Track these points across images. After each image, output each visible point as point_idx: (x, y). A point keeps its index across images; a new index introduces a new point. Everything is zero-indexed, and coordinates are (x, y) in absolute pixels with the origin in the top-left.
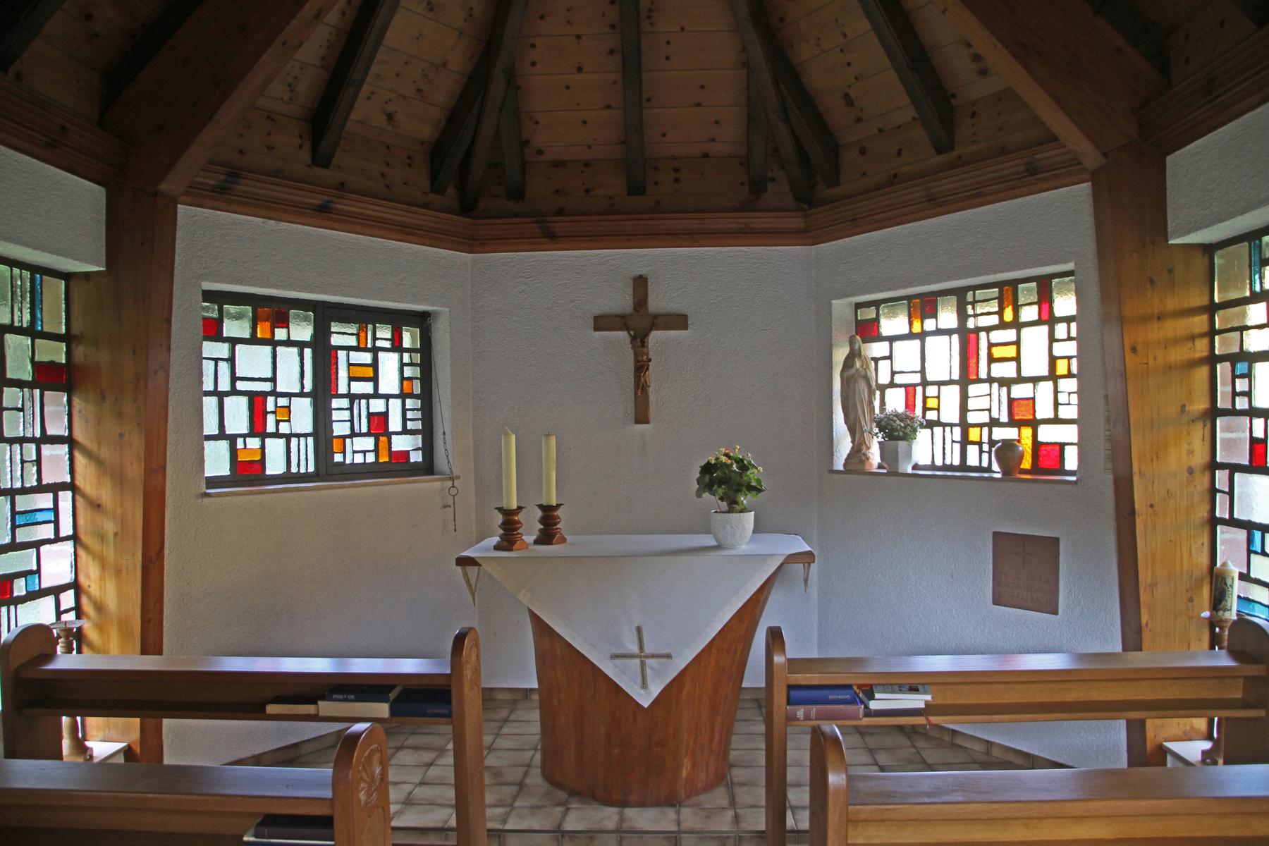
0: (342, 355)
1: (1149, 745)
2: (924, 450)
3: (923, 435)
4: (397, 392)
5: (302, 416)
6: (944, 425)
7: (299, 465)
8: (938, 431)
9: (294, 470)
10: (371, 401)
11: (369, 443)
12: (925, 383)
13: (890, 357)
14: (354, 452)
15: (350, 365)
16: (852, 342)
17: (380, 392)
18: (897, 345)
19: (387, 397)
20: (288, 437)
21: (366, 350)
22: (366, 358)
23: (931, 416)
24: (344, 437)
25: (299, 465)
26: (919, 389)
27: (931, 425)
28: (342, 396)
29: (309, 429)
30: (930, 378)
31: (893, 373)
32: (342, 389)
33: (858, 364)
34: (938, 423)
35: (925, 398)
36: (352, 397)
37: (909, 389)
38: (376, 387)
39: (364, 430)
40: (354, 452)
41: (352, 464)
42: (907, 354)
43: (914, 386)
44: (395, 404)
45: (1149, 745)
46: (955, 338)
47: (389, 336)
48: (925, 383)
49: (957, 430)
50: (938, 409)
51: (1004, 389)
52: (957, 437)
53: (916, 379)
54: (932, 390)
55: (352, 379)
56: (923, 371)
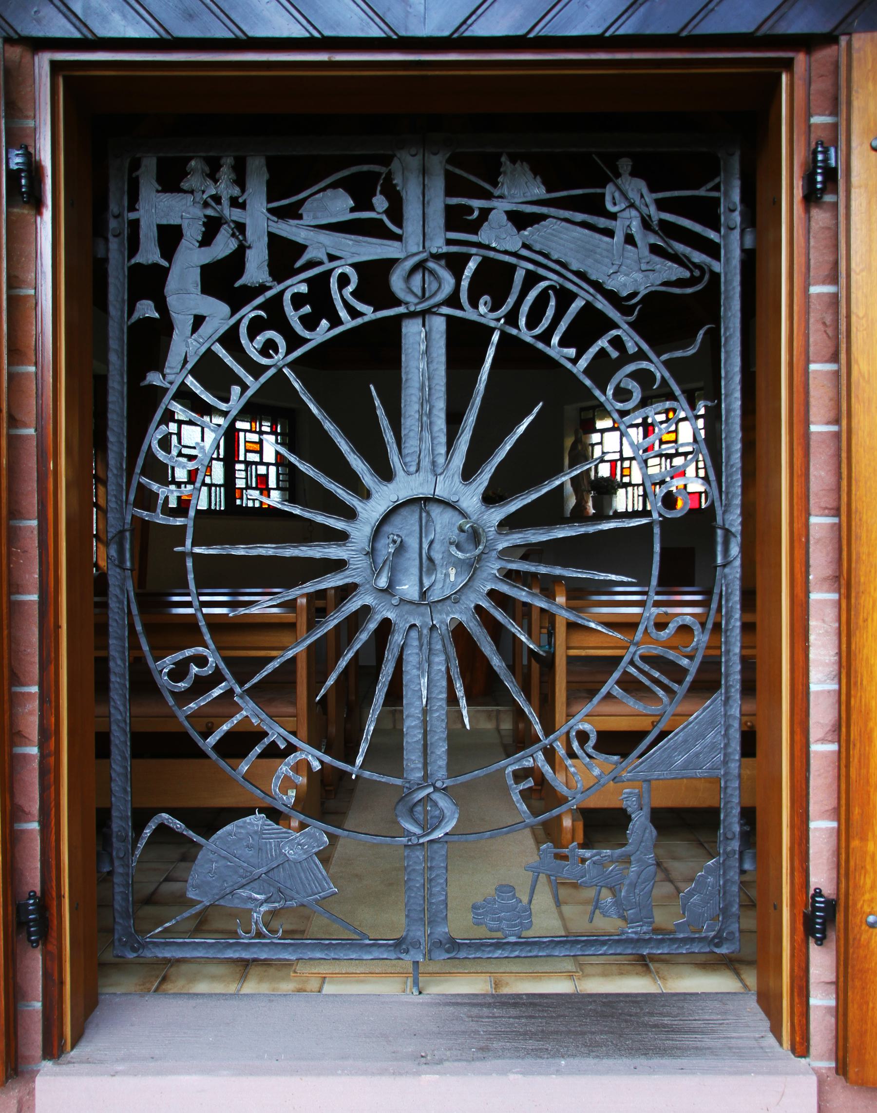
0: (242, 434)
1: (300, 212)
2: (622, 501)
3: (621, 492)
4: (274, 462)
5: (218, 473)
6: (634, 485)
7: (216, 504)
8: (630, 489)
9: (213, 507)
10: (259, 467)
11: (255, 494)
12: (622, 459)
13: (601, 443)
14: (248, 499)
15: (246, 442)
16: (576, 433)
17: (264, 461)
18: (606, 435)
19: (268, 465)
20: (210, 486)
21: (255, 432)
22: (255, 437)
23: (626, 480)
24: (242, 489)
25: (216, 504)
26: (619, 463)
27: (626, 485)
28: (241, 462)
29: (221, 482)
30: (625, 456)
31: (603, 453)
32: (242, 458)
33: (580, 448)
34: (629, 484)
35: (622, 469)
36: (248, 464)
37: (613, 463)
38: (261, 457)
39: (254, 485)
40: (248, 499)
41: (247, 507)
42: (612, 441)
43: (616, 461)
44: (273, 470)
45: (300, 212)
46: (641, 429)
47: (269, 424)
48: (622, 459)
49: (641, 488)
50: (630, 475)
51: (668, 460)
52: (641, 493)
53: (617, 456)
54: (626, 464)
55: (247, 451)
56: (621, 452)
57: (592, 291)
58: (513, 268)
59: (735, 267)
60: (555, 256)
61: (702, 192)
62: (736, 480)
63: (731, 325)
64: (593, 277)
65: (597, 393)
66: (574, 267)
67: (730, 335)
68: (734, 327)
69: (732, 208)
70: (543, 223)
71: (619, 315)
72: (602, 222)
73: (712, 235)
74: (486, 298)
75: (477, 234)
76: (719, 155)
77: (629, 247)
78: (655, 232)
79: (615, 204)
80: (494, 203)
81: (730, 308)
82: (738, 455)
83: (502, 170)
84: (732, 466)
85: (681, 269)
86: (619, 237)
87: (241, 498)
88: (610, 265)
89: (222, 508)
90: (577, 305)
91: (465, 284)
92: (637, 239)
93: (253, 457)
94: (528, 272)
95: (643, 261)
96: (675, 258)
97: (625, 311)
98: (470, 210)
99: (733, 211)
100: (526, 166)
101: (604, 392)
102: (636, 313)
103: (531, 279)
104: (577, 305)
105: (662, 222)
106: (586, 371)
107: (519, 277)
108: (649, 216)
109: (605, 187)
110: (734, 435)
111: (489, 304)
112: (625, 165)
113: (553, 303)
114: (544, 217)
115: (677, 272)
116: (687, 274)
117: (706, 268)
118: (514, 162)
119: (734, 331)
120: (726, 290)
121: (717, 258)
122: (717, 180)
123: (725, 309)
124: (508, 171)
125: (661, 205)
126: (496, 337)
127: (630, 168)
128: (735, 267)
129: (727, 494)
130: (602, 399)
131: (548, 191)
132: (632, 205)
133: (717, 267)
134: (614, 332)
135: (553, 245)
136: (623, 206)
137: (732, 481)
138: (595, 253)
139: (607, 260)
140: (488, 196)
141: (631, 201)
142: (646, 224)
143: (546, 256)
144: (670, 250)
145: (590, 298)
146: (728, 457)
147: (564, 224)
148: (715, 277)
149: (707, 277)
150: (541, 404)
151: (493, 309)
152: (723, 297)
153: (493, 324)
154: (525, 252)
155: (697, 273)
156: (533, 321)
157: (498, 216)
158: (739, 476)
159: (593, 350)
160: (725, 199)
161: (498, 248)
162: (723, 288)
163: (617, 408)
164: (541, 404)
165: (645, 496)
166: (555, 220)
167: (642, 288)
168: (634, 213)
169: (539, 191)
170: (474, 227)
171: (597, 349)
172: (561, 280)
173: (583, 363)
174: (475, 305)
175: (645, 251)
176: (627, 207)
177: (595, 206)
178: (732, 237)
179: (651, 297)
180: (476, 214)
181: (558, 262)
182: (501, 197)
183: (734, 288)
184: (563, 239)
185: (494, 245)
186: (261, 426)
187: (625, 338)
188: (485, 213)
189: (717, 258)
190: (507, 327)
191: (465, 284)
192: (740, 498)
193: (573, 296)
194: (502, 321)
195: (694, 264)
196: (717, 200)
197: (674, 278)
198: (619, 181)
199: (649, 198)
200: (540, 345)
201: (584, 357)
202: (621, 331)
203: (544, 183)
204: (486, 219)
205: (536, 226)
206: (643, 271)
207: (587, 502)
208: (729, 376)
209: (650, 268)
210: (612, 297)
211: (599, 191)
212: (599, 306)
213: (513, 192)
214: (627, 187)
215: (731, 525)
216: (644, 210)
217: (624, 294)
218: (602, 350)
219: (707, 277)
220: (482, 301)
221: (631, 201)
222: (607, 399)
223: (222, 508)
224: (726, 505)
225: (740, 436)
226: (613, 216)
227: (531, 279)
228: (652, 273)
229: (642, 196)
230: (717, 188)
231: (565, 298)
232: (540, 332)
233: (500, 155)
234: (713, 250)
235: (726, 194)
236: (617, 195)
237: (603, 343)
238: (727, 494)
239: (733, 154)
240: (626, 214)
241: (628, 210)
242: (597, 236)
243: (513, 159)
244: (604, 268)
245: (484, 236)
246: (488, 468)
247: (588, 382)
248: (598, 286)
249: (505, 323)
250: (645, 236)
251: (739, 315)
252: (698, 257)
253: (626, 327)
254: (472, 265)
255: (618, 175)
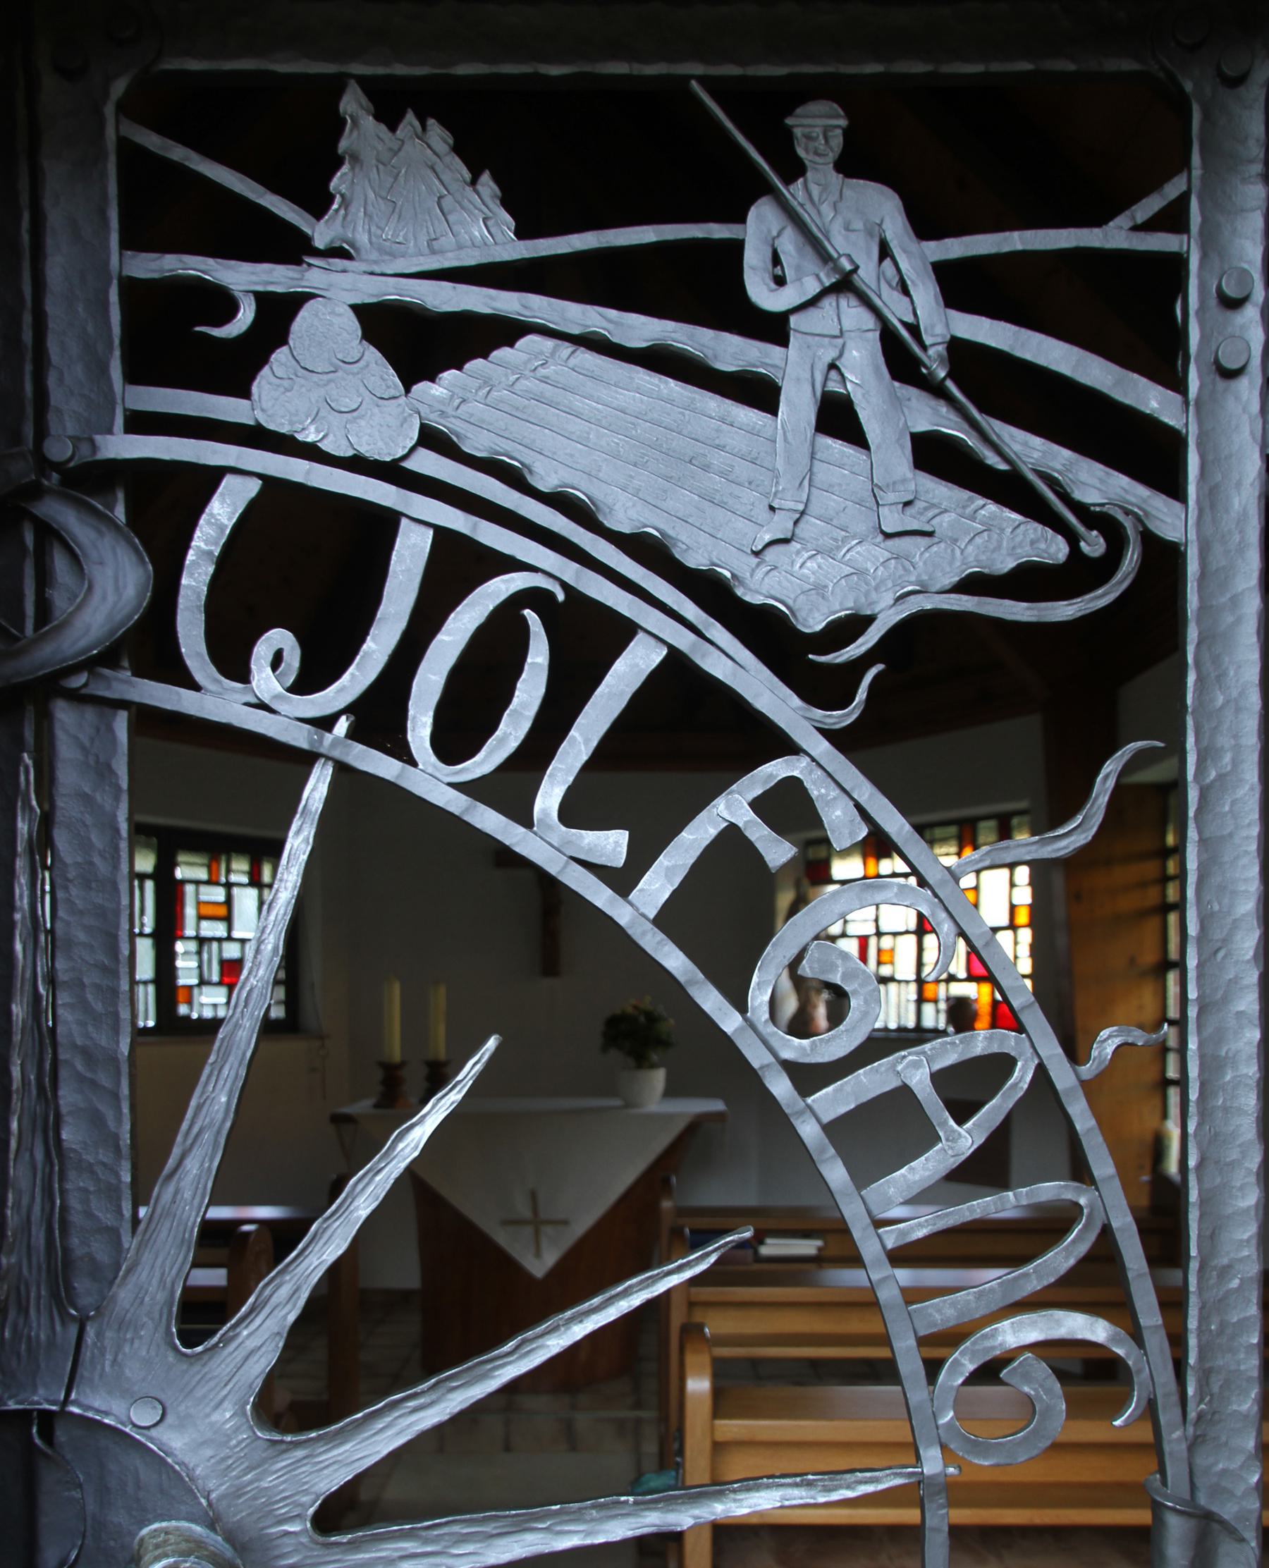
0: (190, 889)
12: (879, 934)
15: (199, 903)
16: (798, 885)
22: (218, 894)
23: (885, 971)
24: (190, 988)
32: (190, 931)
35: (879, 951)
36: (202, 941)
37: (863, 941)
39: (215, 978)
48: (879, 934)
50: (892, 963)
54: (886, 942)
55: (201, 917)
57: (690, 610)
58: (383, 525)
59: (1242, 520)
60: (546, 481)
61: (1115, 236)
62: (1242, 1324)
63: (1224, 741)
64: (695, 560)
65: (711, 1000)
66: (621, 522)
67: (1221, 777)
68: (1237, 748)
69: (1231, 291)
70: (502, 354)
71: (796, 701)
72: (730, 351)
73: (1151, 399)
74: (279, 639)
75: (245, 394)
76: (1188, 87)
77: (834, 447)
78: (938, 391)
79: (780, 281)
80: (312, 276)
81: (1221, 677)
82: (1249, 1230)
83: (343, 145)
84: (1225, 1272)
85: (1034, 529)
86: (799, 405)
87: (189, 1002)
88: (762, 513)
89: (151, 1023)
90: (632, 668)
91: (196, 577)
92: (863, 416)
93: (214, 929)
94: (444, 537)
95: (891, 497)
96: (1012, 490)
97: (821, 688)
98: (224, 305)
99: (1233, 304)
100: (438, 135)
101: (739, 1002)
102: (862, 694)
103: (456, 567)
104: (632, 668)
105: (959, 350)
106: (667, 920)
107: (410, 555)
108: (914, 329)
109: (740, 217)
110: (1234, 1155)
111: (293, 658)
112: (819, 129)
113: (538, 655)
114: (507, 331)
115: (1015, 540)
116: (1055, 549)
117: (1128, 523)
118: (389, 117)
119: (1235, 763)
120: (1202, 608)
121: (1173, 487)
122: (1173, 189)
123: (1200, 679)
124: (368, 156)
125: (962, 286)
126: (317, 788)
127: (837, 141)
128: (1242, 520)
129: (1205, 1377)
130: (730, 1022)
131: (523, 233)
132: (845, 285)
133: (1169, 519)
134: (777, 769)
135: (545, 438)
136: (812, 288)
137: (1223, 1326)
138: (706, 468)
139: (749, 496)
140: (293, 248)
141: (841, 258)
142: (900, 358)
143: (514, 478)
144: (992, 460)
145: (683, 640)
146: (1211, 1239)
147: (587, 358)
148: (1164, 560)
149: (1131, 559)
150: (492, 1043)
151: (307, 683)
152: (1192, 634)
153: (300, 737)
154: (428, 463)
155: (1093, 545)
156: (459, 732)
157: (326, 328)
158: (1253, 1310)
159: (697, 835)
160: (1204, 257)
161: (326, 446)
162: (1193, 601)
163: (787, 1055)
164: (492, 1043)
165: (921, 1000)
166: (549, 343)
167: (888, 598)
168: (853, 314)
169: (486, 231)
170: (236, 368)
171: (713, 832)
172: (570, 571)
173: (657, 886)
174: (238, 670)
175: (894, 458)
176: (825, 292)
177: (705, 285)
178: (1231, 405)
179: (916, 634)
180: (245, 316)
181: (561, 502)
182: (338, 253)
183: (1235, 601)
184: (576, 413)
185: (310, 436)
186: (228, 871)
187: (818, 789)
188: (278, 313)
189: (1173, 487)
190: (359, 748)
191: (196, 577)
192: (1254, 1392)
193: (621, 632)
194: (342, 726)
195: (1080, 509)
196: (1175, 266)
197: (1005, 564)
198: (796, 193)
199: (916, 257)
200: (489, 820)
201: (663, 861)
202: (804, 761)
203: (508, 203)
204: (281, 338)
205: (476, 365)
206: (888, 536)
207: (815, 1007)
208: (1217, 935)
209: (915, 526)
210: (766, 632)
211: (718, 231)
212: (715, 667)
213: (388, 233)
214: (826, 209)
215: (1217, 1491)
216: (896, 309)
217: (813, 621)
218: (732, 833)
219: (1131, 559)
220: (262, 651)
221: (841, 258)
222: (752, 1026)
223: (151, 1023)
224: (1200, 1416)
225: (1255, 1159)
226: (773, 329)
227: (456, 567)
228: (923, 542)
229: (885, 252)
230: (1173, 218)
231: (588, 638)
232: (487, 768)
233: (336, 86)
234: (1153, 455)
235: (1210, 244)
236: (789, 244)
237: (733, 807)
238: (1205, 1377)
239: (1236, 82)
240: (823, 319)
241: (828, 303)
242: (713, 403)
243: (390, 105)
244: (740, 524)
245: (274, 398)
246: (284, 1292)
247: (674, 960)
248: (712, 592)
249: (352, 734)
250: (897, 403)
251: (1254, 700)
252: (1096, 483)
253: (821, 747)
254: (223, 511)
255: (793, 170)
